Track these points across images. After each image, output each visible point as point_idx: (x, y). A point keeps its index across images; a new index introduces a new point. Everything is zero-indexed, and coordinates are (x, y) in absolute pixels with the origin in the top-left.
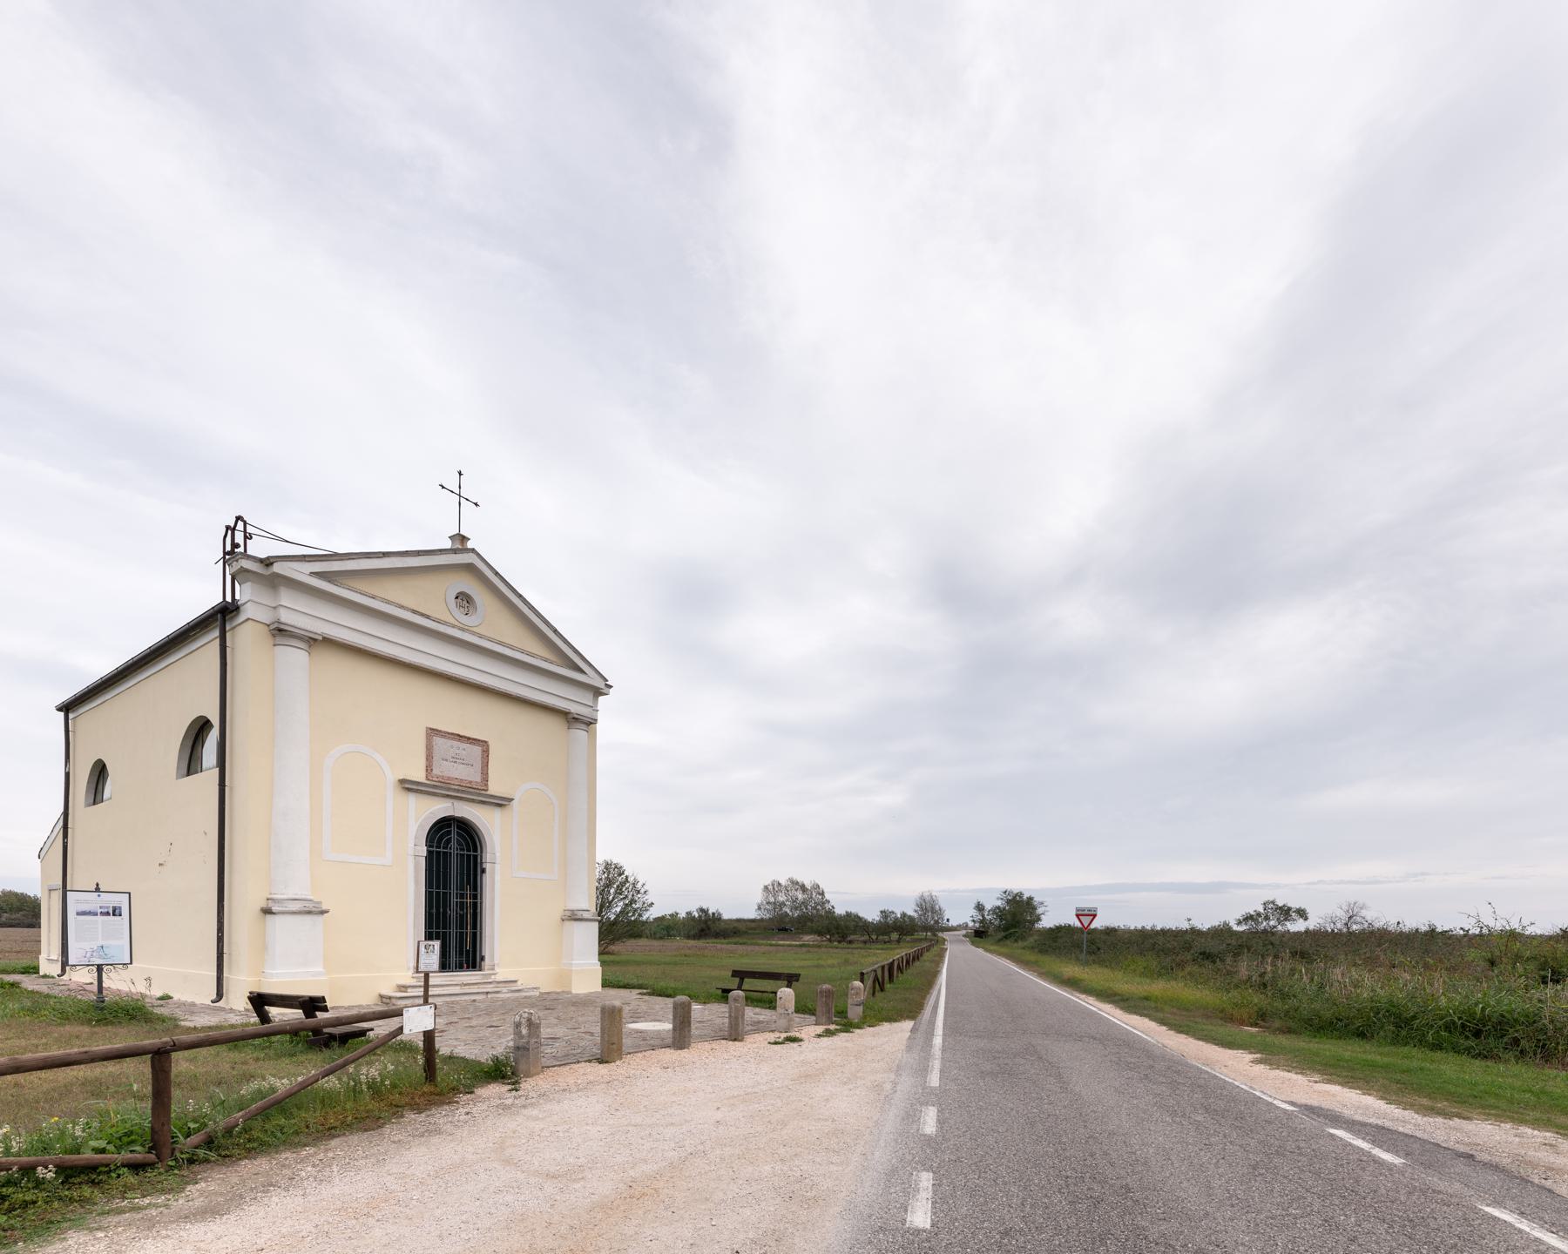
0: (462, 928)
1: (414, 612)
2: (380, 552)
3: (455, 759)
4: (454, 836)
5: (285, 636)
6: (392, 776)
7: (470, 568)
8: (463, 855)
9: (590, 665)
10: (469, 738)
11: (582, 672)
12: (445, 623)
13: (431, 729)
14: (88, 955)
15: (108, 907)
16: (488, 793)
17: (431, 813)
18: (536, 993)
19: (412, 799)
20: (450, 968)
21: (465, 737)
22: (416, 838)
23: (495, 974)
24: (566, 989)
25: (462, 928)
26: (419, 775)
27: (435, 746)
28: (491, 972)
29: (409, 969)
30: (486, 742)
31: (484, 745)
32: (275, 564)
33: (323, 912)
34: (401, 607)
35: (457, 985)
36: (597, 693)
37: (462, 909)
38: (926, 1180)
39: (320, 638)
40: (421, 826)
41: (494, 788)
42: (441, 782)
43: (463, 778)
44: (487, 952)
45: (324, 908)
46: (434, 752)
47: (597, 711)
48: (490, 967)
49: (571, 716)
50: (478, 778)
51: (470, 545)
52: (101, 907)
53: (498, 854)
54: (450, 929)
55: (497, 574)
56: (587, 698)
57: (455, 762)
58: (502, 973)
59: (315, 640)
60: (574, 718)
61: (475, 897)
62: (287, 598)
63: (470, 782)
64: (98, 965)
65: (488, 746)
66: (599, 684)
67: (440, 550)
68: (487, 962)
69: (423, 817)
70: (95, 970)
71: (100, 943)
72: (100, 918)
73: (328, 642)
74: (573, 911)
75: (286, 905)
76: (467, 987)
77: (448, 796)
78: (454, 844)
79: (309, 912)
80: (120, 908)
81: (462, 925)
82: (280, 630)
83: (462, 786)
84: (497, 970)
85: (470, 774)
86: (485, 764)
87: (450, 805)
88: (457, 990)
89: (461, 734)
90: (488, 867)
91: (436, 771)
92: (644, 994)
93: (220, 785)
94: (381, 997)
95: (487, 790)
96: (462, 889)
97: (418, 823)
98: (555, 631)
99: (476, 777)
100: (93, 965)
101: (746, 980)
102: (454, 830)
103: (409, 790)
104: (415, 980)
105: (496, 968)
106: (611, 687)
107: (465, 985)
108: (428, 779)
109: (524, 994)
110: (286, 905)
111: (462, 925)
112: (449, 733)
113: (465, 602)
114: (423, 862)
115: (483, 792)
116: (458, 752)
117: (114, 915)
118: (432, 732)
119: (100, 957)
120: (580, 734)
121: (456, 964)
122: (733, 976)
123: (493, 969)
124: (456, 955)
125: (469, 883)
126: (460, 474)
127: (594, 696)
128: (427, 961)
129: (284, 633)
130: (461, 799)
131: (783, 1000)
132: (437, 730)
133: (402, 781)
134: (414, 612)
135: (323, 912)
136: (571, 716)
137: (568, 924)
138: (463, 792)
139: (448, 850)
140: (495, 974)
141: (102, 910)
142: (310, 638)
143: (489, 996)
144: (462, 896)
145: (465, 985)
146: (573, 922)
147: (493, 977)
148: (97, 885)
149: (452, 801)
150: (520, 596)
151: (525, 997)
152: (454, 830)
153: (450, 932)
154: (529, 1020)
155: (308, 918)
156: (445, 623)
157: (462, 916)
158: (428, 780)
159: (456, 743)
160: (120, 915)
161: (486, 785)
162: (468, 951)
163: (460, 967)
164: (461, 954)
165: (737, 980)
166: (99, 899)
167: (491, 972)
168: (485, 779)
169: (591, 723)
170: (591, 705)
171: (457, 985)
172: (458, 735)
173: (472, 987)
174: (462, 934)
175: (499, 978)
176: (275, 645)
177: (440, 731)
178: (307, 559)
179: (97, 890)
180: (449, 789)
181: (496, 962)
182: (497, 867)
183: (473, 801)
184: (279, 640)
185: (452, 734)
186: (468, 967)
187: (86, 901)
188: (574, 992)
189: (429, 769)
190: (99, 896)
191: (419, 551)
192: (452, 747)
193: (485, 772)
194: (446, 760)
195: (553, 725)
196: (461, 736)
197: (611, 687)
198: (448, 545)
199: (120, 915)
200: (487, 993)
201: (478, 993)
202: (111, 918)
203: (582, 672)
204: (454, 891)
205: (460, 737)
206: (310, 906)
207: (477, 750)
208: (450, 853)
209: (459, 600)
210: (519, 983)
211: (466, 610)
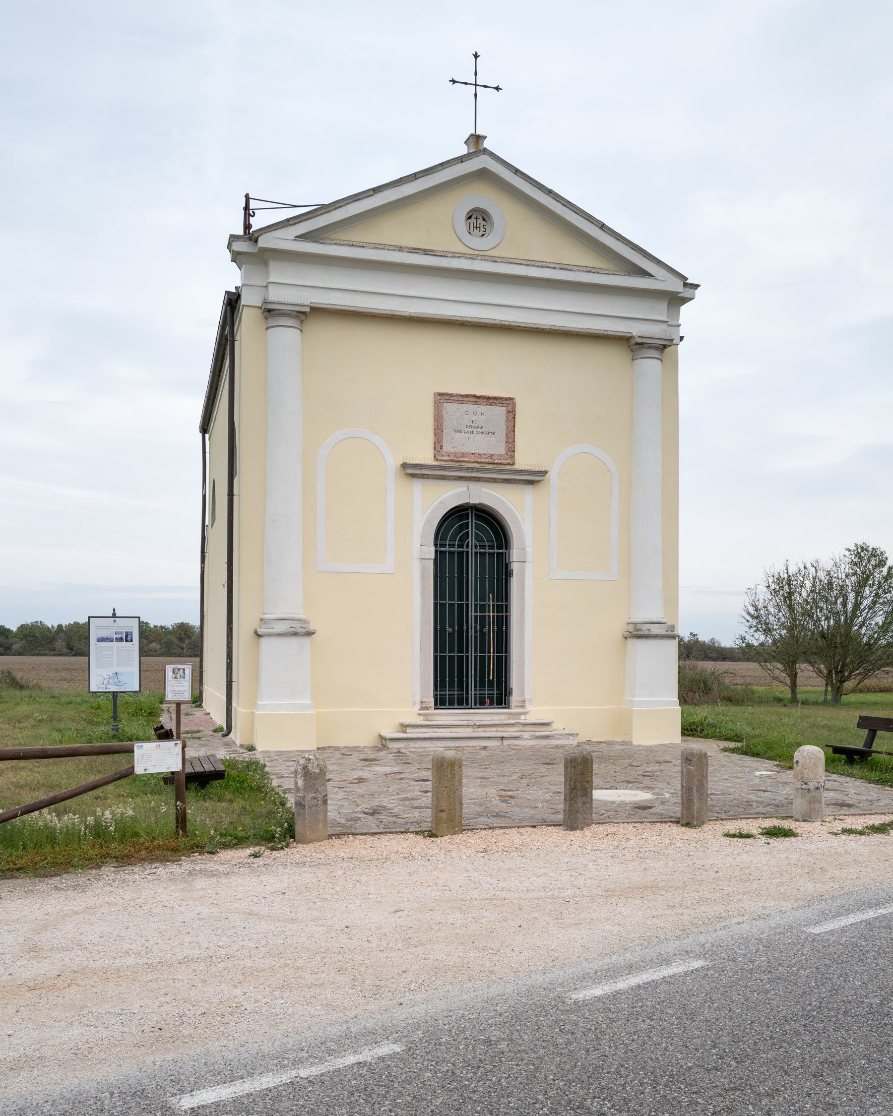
0: (483, 650)
1: (414, 250)
2: (369, 190)
3: (472, 429)
4: (472, 530)
5: (274, 316)
6: (393, 462)
7: (483, 174)
8: (453, 553)
9: (658, 262)
10: (489, 398)
11: (645, 274)
12: (456, 255)
13: (440, 394)
14: (106, 682)
15: (122, 633)
16: (516, 467)
17: (440, 503)
18: (573, 742)
19: (418, 488)
20: (467, 704)
21: (484, 397)
22: (422, 536)
23: (526, 713)
24: (626, 738)
25: (483, 650)
26: (425, 455)
27: (445, 416)
28: (521, 710)
29: (414, 704)
30: (511, 399)
31: (508, 403)
32: (260, 239)
33: (310, 634)
34: (401, 249)
35: (468, 726)
36: (676, 300)
37: (483, 626)
38: (397, 1048)
39: (308, 309)
40: (428, 521)
41: (524, 460)
42: (453, 461)
43: (482, 452)
44: (514, 683)
45: (312, 628)
46: (445, 423)
47: (679, 326)
48: (520, 704)
49: (633, 342)
50: (500, 449)
51: (486, 144)
52: (116, 633)
53: (529, 550)
54: (467, 652)
55: (517, 171)
56: (659, 311)
57: (471, 432)
58: (535, 712)
59: (304, 313)
60: (637, 344)
61: (500, 609)
62: (278, 273)
63: (491, 456)
64: (113, 692)
65: (514, 404)
66: (675, 286)
67: (442, 164)
68: (514, 699)
69: (431, 508)
70: (111, 697)
71: (116, 669)
72: (115, 644)
73: (317, 312)
74: (635, 624)
75: (272, 626)
76: (481, 729)
77: (461, 478)
78: (472, 540)
79: (295, 634)
80: (131, 633)
81: (483, 647)
82: (269, 311)
83: (480, 463)
84: (529, 707)
85: (494, 446)
86: (511, 428)
87: (465, 489)
88: (468, 732)
89: (478, 394)
90: (515, 567)
91: (447, 448)
92: (733, 751)
93: (229, 495)
94: (381, 737)
95: (513, 464)
96: (483, 599)
97: (425, 519)
98: (603, 227)
99: (500, 449)
100: (109, 692)
101: (879, 733)
102: (472, 521)
103: (413, 476)
104: (422, 718)
105: (527, 704)
106: (696, 286)
107: (479, 726)
108: (436, 460)
109: (554, 742)
110: (272, 626)
111: (483, 647)
112: (462, 396)
113: (480, 221)
114: (431, 565)
115: (509, 467)
116: (474, 418)
117: (126, 641)
118: (442, 398)
119: (115, 684)
120: (650, 366)
121: (475, 698)
122: (860, 726)
123: (523, 707)
124: (475, 686)
125: (491, 590)
126: (476, 56)
127: (669, 305)
128: (176, 689)
129: (273, 313)
130: (478, 479)
131: (800, 764)
132: (447, 394)
133: (405, 466)
134: (414, 250)
135: (310, 634)
136: (633, 342)
137: (632, 642)
138: (478, 470)
139: (465, 549)
140: (526, 713)
141: (117, 636)
142: (299, 312)
143: (506, 742)
144: (483, 608)
145: (479, 726)
146: (635, 641)
147: (523, 717)
148: (114, 610)
149: (466, 483)
150: (549, 192)
151: (557, 747)
152: (472, 521)
153: (467, 657)
154: (305, 768)
155: (295, 640)
156: (456, 255)
157: (483, 634)
158: (437, 460)
159: (471, 407)
160: (132, 641)
161: (513, 457)
162: (491, 683)
163: (481, 703)
164: (482, 685)
165: (864, 733)
166: (115, 625)
167: (521, 710)
168: (511, 450)
169: (665, 347)
170: (665, 319)
171: (468, 726)
172: (475, 396)
173: (488, 729)
174: (482, 658)
175: (530, 719)
176: (267, 329)
177: (451, 395)
178: (291, 222)
179: (114, 615)
180: (460, 469)
181: (527, 697)
182: (529, 567)
183: (494, 480)
184: (272, 322)
185: (467, 396)
186: (491, 703)
187: (105, 628)
188: (635, 743)
189: (438, 445)
190: (115, 621)
191: (415, 174)
192: (467, 413)
193: (510, 440)
194: (460, 431)
195: (613, 357)
196: (479, 397)
197: (696, 286)
198: (463, 150)
199: (132, 641)
200: (502, 738)
201: (489, 738)
202: (124, 643)
203: (645, 274)
204: (472, 602)
205: (477, 399)
206: (297, 626)
207: (500, 411)
208: (468, 552)
209: (473, 220)
210: (554, 726)
211: (482, 229)
